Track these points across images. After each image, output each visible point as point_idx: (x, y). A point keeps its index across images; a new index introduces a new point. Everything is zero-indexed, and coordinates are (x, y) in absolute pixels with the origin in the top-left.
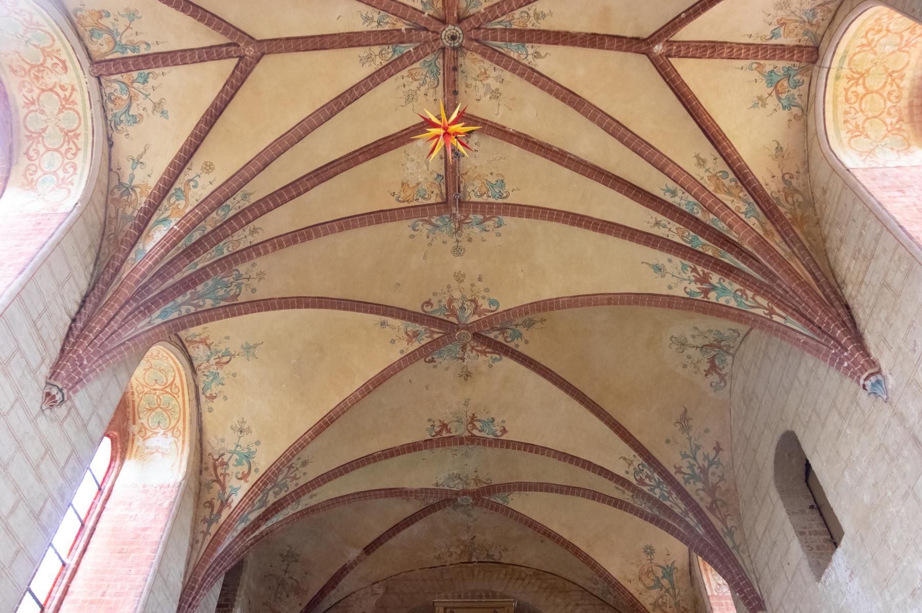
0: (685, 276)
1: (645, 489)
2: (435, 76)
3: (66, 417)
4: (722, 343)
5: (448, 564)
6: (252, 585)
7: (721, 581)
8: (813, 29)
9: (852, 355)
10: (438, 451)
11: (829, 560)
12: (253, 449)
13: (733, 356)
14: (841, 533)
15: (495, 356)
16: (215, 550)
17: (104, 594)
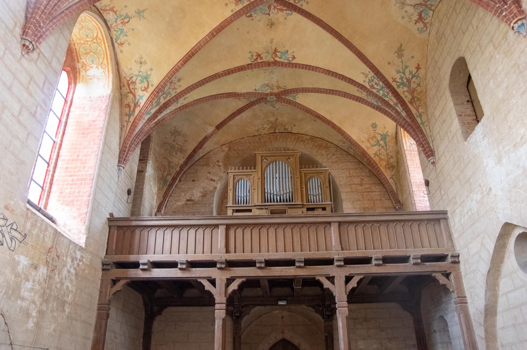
1: (374, 91)
3: (38, 59)
4: (428, 3)
5: (263, 134)
6: (157, 149)
7: (413, 142)
9: (510, 7)
10: (255, 70)
11: (473, 129)
12: (149, 73)
13: (434, 11)
14: (483, 115)
15: (288, 12)
16: (134, 130)
17: (78, 156)
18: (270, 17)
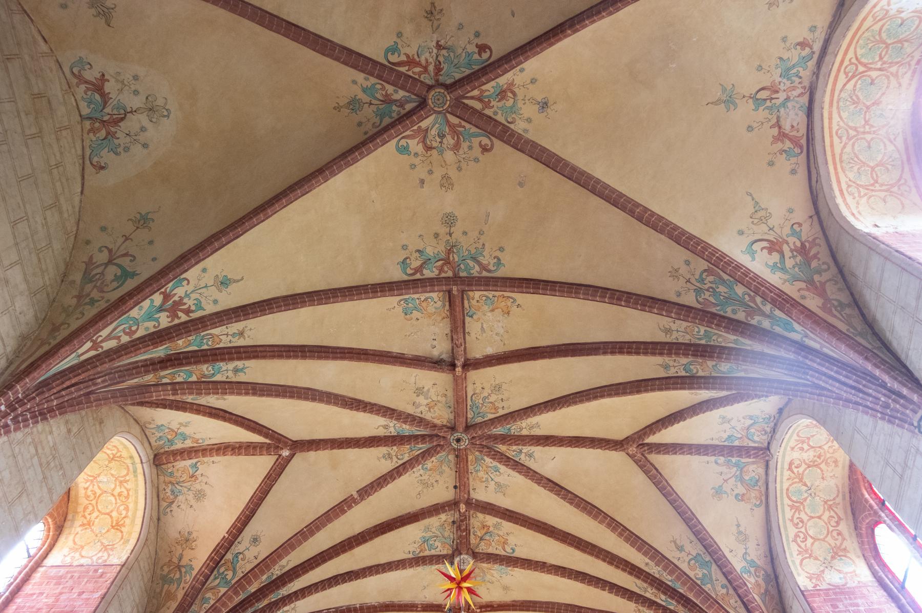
0: (194, 296)
2: (474, 404)
4: (103, 133)
8: (168, 479)
15: (394, 58)
18: (435, 37)
